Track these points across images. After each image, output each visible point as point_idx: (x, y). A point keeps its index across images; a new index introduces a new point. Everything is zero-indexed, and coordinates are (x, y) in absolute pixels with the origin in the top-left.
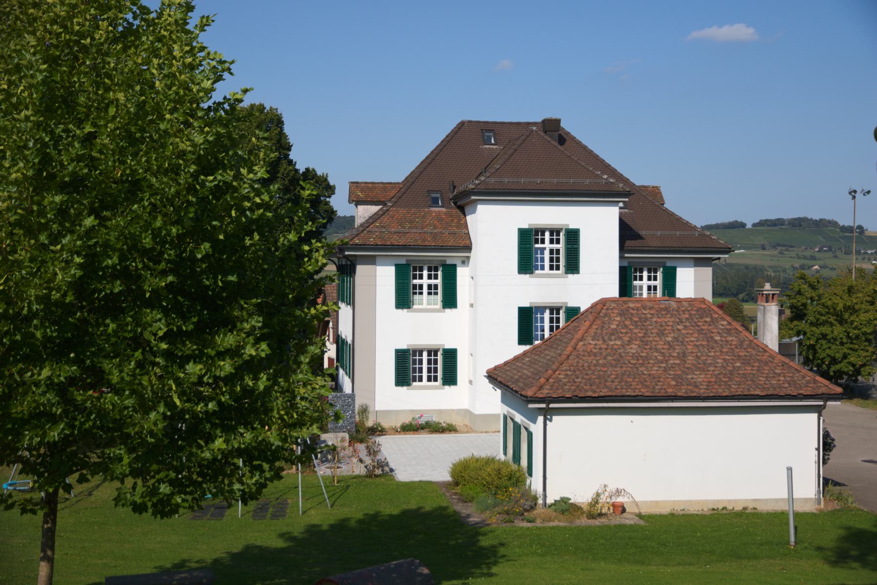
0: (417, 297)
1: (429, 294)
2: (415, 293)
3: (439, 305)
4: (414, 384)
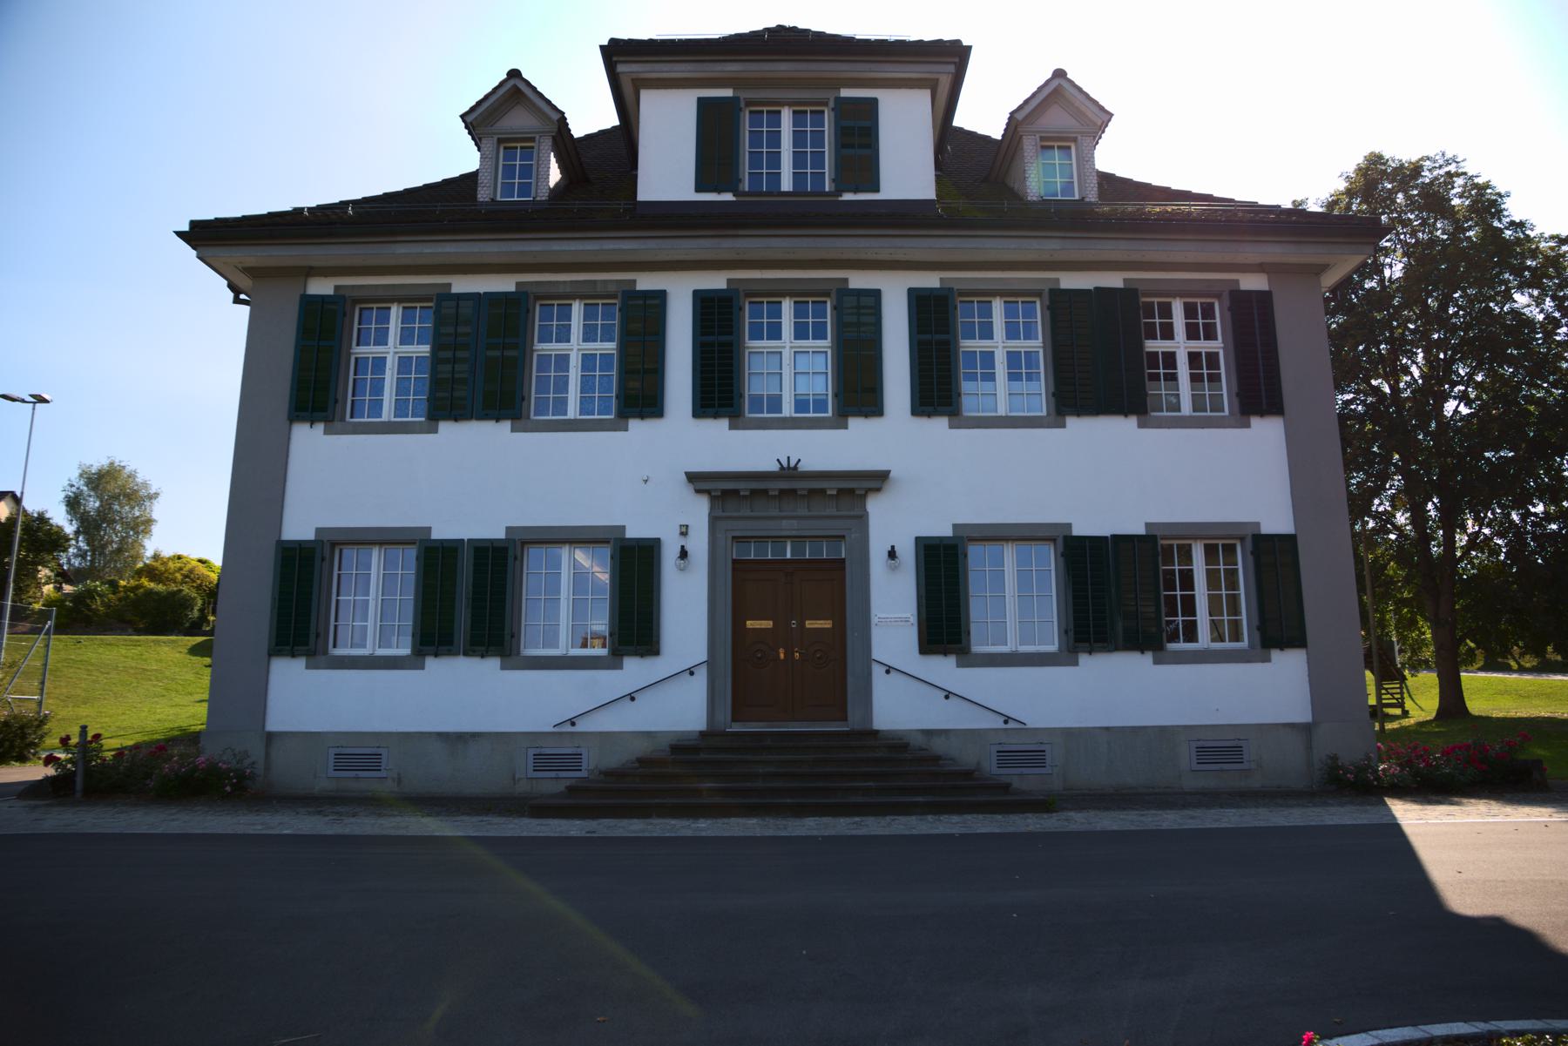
0: (1163, 389)
1: (1014, 377)
2: (1156, 377)
3: (1040, 407)
4: (1172, 646)
